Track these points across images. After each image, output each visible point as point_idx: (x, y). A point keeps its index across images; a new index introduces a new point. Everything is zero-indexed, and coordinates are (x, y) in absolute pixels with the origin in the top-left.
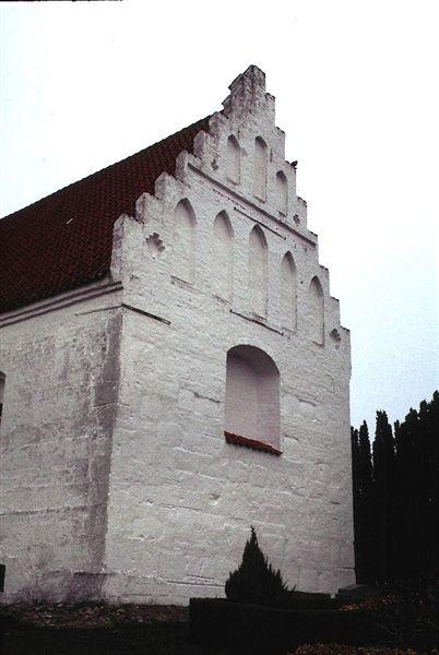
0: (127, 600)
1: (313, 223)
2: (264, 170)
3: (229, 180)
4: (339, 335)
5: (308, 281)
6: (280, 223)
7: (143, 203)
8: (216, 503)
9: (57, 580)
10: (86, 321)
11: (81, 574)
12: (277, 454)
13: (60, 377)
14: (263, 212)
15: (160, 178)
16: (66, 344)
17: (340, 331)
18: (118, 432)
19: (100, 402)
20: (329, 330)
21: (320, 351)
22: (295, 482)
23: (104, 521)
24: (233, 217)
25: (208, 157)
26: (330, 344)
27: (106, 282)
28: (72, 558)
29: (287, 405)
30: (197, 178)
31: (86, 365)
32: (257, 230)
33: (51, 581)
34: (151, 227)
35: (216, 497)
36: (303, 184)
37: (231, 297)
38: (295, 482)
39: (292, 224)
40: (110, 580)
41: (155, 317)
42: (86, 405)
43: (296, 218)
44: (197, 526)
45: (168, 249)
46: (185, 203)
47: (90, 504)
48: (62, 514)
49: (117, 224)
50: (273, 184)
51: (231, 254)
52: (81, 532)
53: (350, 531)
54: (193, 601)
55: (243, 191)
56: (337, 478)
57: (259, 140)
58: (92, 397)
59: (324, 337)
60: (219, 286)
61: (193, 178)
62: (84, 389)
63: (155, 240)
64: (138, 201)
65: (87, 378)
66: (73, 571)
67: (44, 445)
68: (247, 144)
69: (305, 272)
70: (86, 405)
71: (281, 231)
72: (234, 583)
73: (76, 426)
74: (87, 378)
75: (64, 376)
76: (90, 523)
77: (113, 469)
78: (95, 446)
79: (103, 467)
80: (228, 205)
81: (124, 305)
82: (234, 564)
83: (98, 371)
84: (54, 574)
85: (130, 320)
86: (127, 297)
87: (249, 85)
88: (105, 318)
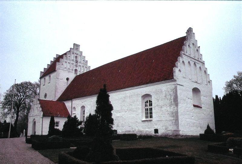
0: (183, 134)
1: (204, 59)
2: (194, 50)
3: (189, 55)
4: (210, 82)
5: (204, 72)
6: (198, 61)
7: (177, 64)
8: (193, 118)
9: (170, 131)
10: (168, 86)
11: (175, 130)
12: (201, 108)
13: (165, 97)
14: (195, 59)
15: (178, 58)
16: (165, 90)
17: (210, 81)
18: (179, 107)
19: (174, 101)
20: (208, 81)
21: (207, 86)
22: (205, 113)
23: (178, 122)
24: (191, 62)
25: (185, 51)
26: (208, 84)
27: (173, 79)
28: (41, 134)
29: (202, 97)
30: (184, 56)
31: (170, 95)
32: (195, 64)
33: (169, 131)
34: (179, 68)
35: (193, 117)
36: (202, 51)
37: (192, 78)
38: (205, 113)
39: (200, 60)
40: (180, 131)
41: (181, 85)
42: (172, 102)
43: (201, 59)
44: (191, 122)
45: (182, 72)
46: (183, 62)
47: (175, 119)
48: (169, 121)
49: (174, 69)
50: (196, 53)
51: (191, 70)
52: (174, 124)
53: (214, 121)
54: (200, 134)
55: (192, 56)
56: (211, 111)
57: (193, 44)
58: (173, 100)
59: (207, 83)
60: (190, 77)
61: (184, 56)
62: (170, 99)
63: (180, 70)
64: (176, 63)
65: (171, 97)
66: (173, 130)
67: (163, 109)
68: (191, 46)
69: (203, 70)
70: (172, 102)
71: (199, 62)
72: (206, 131)
73: (170, 106)
74: (171, 97)
75: (165, 96)
76: (175, 122)
77: (179, 113)
78: (174, 109)
79: (177, 113)
80: (189, 60)
81: (177, 84)
82: (205, 128)
83: (173, 96)
84: (169, 130)
85: (178, 86)
86: (178, 82)
87: (190, 31)
88: (173, 86)
